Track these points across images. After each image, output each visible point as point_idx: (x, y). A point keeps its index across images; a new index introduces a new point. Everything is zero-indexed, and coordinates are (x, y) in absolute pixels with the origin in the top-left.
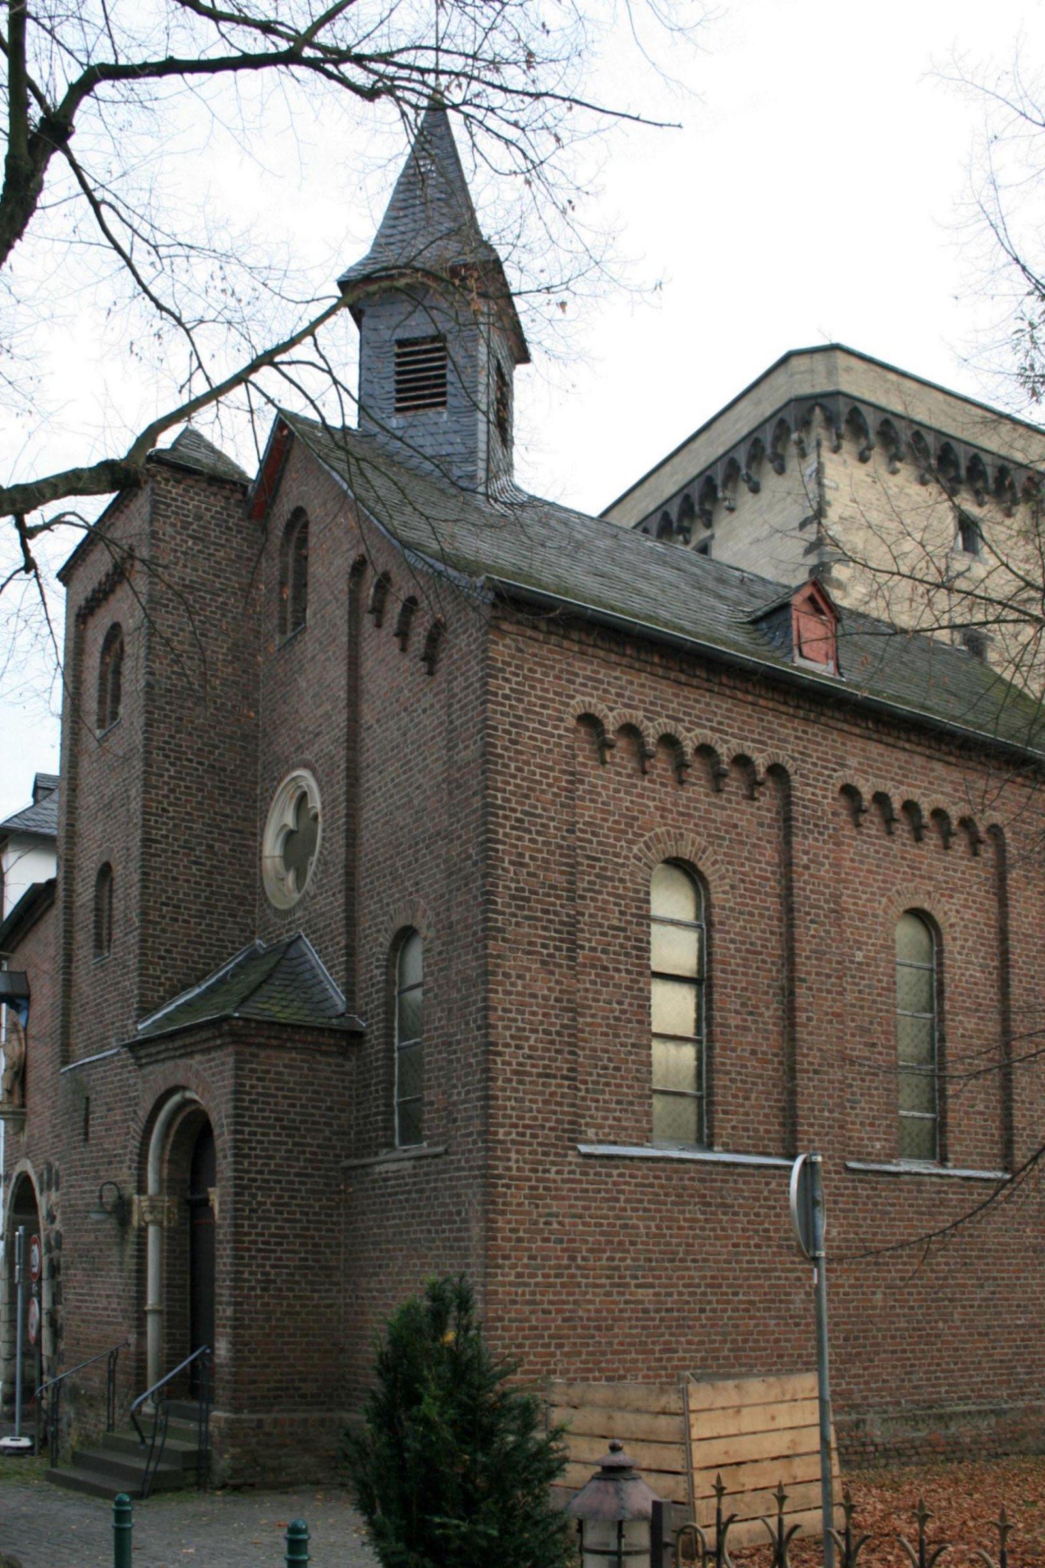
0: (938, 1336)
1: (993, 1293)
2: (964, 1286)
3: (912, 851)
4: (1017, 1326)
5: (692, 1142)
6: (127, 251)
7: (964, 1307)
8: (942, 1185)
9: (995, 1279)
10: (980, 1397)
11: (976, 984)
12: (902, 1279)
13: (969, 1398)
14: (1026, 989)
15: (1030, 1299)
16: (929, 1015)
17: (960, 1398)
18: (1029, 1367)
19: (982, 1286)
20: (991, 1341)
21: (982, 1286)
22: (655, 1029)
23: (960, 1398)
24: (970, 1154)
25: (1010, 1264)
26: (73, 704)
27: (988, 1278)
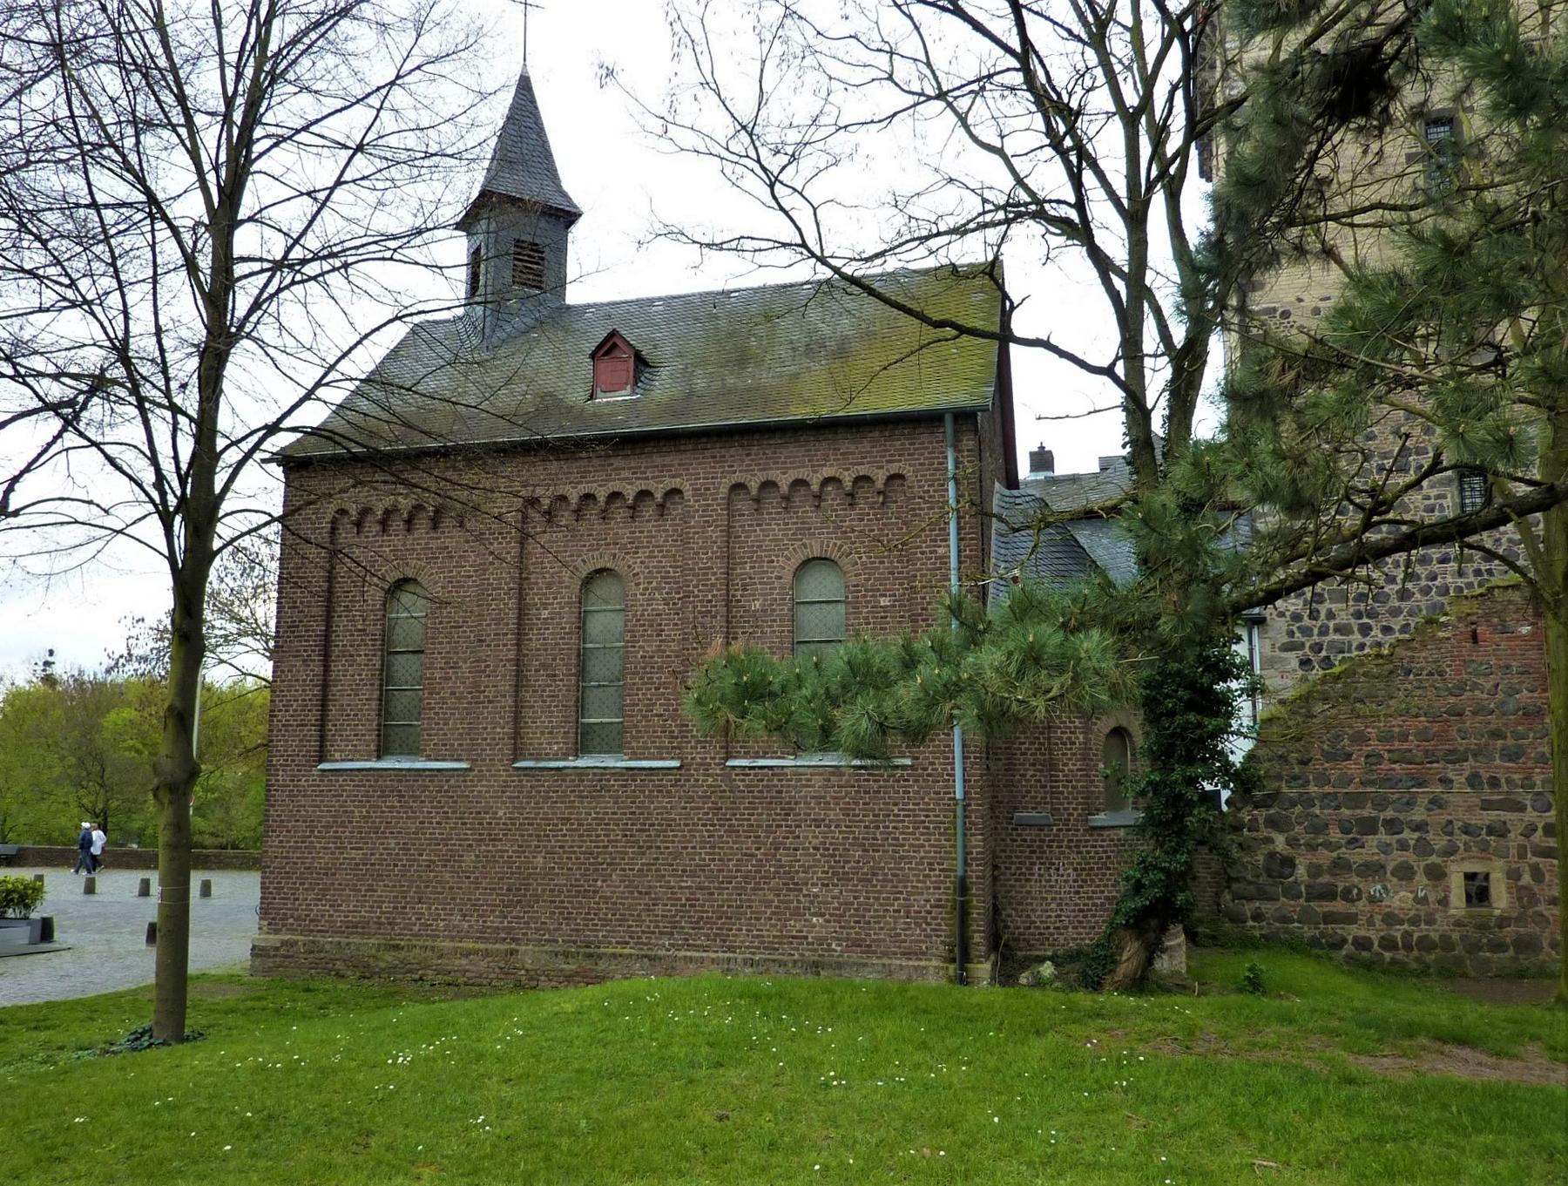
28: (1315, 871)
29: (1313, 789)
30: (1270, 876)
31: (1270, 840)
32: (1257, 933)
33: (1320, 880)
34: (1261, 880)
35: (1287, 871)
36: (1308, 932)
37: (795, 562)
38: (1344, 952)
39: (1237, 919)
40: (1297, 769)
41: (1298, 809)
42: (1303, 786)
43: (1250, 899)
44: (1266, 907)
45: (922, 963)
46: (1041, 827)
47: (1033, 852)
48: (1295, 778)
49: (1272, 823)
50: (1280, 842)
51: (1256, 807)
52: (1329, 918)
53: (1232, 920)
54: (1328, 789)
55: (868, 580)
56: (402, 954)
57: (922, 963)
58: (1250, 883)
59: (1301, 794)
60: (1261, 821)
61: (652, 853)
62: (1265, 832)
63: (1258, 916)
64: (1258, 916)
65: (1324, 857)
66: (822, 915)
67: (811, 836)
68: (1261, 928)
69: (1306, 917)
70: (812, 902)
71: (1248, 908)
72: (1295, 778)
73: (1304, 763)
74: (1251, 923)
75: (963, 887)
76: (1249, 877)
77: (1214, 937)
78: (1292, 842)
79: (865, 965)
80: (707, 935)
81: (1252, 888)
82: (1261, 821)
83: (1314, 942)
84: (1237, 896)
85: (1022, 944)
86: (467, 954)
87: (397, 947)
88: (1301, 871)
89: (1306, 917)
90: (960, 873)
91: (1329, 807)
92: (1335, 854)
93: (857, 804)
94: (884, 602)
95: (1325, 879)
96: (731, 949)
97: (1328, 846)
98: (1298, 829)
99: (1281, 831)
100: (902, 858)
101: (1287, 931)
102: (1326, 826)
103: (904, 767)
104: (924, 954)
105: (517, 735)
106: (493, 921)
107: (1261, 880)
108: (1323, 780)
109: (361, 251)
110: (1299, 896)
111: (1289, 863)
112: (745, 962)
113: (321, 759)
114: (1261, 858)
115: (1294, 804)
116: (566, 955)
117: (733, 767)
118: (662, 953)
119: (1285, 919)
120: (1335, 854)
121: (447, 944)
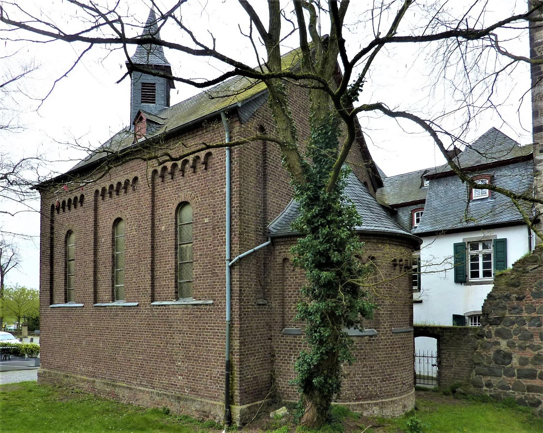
0: (116, 359)
1: (132, 346)
2: (123, 343)
3: (112, 201)
4: (139, 359)
5: (536, 125)
6: (179, 19)
7: (123, 350)
8: (117, 309)
9: (132, 341)
10: (127, 382)
11: (134, 236)
12: (107, 339)
13: (124, 381)
14: (143, 234)
15: (143, 350)
16: (117, 253)
17: (122, 381)
18: (144, 375)
19: (128, 343)
20: (131, 363)
21: (128, 343)
22: (529, 65)
23: (122, 381)
24: (131, 297)
25: (137, 336)
26: (181, 134)
27: (130, 341)
28: (524, 361)
29: (525, 315)
30: (496, 363)
31: (498, 343)
32: (488, 394)
33: (526, 367)
34: (491, 365)
35: (507, 361)
36: (518, 395)
37: (176, 206)
38: (539, 409)
39: (478, 386)
40: (515, 303)
41: (516, 325)
42: (518, 313)
43: (485, 375)
44: (494, 380)
45: (215, 403)
46: (295, 336)
47: (291, 349)
48: (514, 308)
49: (499, 333)
50: (503, 344)
51: (491, 325)
52: (530, 389)
53: (475, 386)
54: (534, 315)
55: (201, 210)
56: (69, 379)
57: (215, 403)
58: (485, 366)
59: (517, 318)
60: (493, 332)
61: (131, 344)
62: (495, 339)
63: (489, 385)
64: (489, 385)
65: (530, 354)
66: (182, 375)
67: (178, 338)
68: (491, 391)
69: (517, 387)
70: (178, 369)
71: (484, 380)
72: (514, 308)
73: (519, 299)
74: (485, 388)
75: (229, 366)
76: (485, 363)
77: (464, 394)
78: (511, 345)
79: (195, 401)
80: (146, 381)
81: (486, 369)
82: (493, 332)
83: (521, 402)
84: (478, 373)
85: (285, 396)
86: (84, 381)
87: (67, 376)
88: (515, 361)
89: (517, 387)
90: (227, 359)
91: (534, 325)
92: (536, 353)
93: (193, 323)
94: (206, 220)
95: (530, 366)
96: (154, 388)
97: (532, 347)
98: (514, 337)
99: (504, 338)
100: (209, 350)
101: (505, 394)
102: (532, 336)
103: (210, 305)
104: (217, 398)
105: (95, 293)
106: (91, 369)
107: (491, 365)
108: (531, 309)
109: (148, 97)
110: (513, 375)
111: (509, 356)
112: (157, 393)
113: (52, 303)
114: (492, 353)
115: (513, 323)
116: (108, 384)
117: (153, 305)
118: (133, 387)
119: (505, 388)
120: (536, 353)
121: (79, 376)
